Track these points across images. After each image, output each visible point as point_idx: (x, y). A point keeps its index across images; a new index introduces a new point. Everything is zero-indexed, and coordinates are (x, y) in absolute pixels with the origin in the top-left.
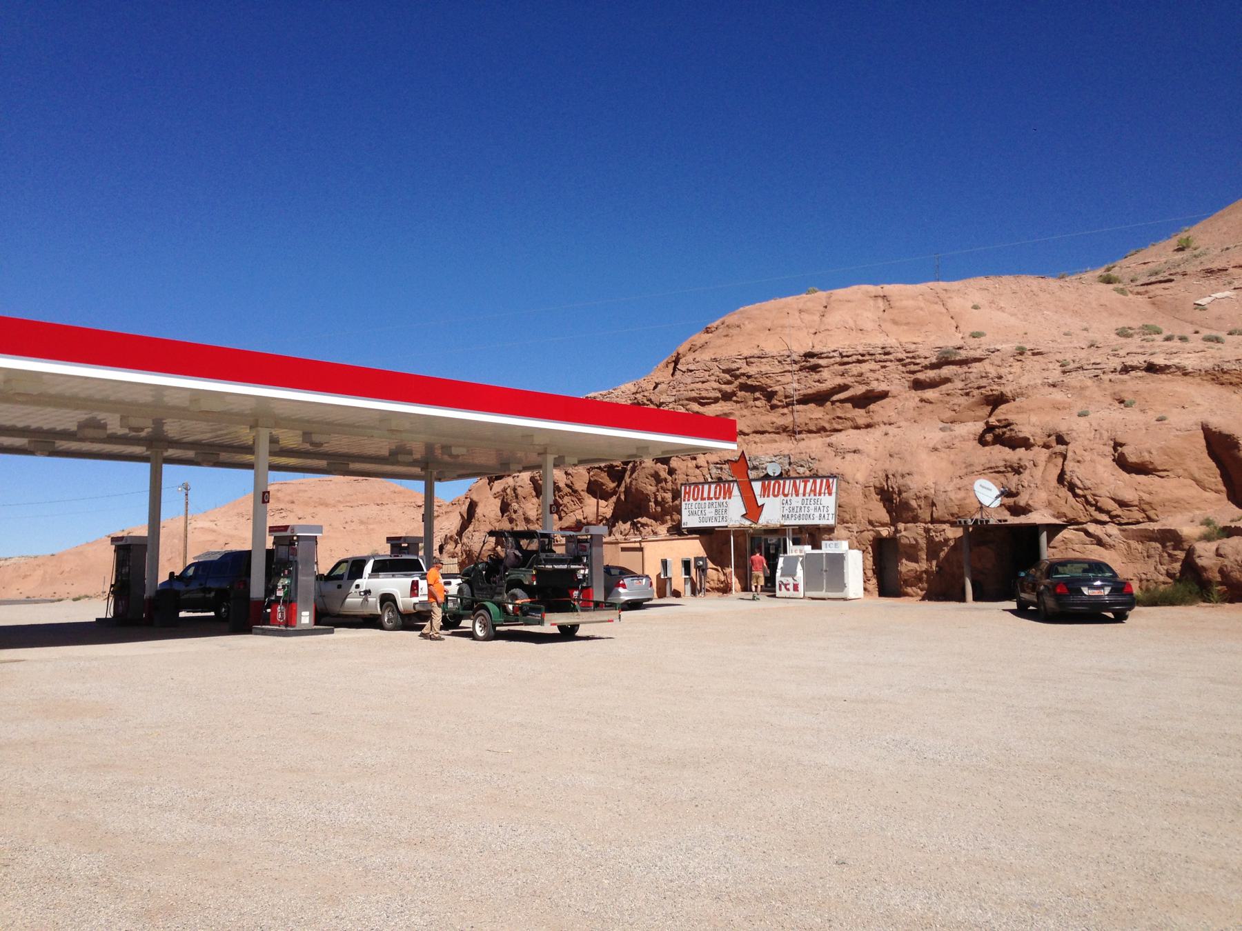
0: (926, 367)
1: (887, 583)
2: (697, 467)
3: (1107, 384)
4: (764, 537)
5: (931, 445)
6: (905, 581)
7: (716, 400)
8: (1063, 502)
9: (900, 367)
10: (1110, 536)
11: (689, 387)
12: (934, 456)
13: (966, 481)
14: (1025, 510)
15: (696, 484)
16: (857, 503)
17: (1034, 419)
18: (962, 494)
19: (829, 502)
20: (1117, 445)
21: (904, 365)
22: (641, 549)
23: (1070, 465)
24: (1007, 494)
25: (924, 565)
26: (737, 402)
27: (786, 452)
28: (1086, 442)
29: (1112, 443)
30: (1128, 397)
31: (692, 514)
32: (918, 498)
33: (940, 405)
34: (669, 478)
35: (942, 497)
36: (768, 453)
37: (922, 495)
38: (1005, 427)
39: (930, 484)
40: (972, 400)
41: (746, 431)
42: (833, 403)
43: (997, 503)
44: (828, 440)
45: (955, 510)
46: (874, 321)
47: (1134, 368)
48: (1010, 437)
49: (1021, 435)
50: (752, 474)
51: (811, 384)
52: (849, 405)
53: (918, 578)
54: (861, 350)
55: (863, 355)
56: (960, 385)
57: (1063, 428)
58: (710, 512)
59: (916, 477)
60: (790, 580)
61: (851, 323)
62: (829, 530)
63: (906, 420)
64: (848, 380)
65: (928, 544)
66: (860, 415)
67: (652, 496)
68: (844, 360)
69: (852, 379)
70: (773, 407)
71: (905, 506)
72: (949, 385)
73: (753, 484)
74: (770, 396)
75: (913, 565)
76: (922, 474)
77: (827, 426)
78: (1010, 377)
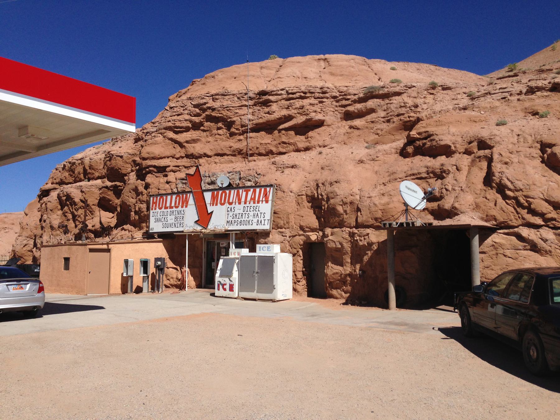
0: (355, 102)
1: (315, 284)
2: (168, 182)
3: (515, 103)
4: (217, 241)
5: (358, 158)
6: (330, 283)
7: (187, 129)
8: (492, 204)
9: (334, 103)
10: (545, 241)
11: (168, 119)
12: (360, 167)
13: (389, 187)
14: (452, 213)
15: (167, 194)
16: (290, 211)
17: (453, 130)
18: (385, 199)
19: (266, 208)
20: (544, 146)
21: (337, 101)
22: (108, 250)
23: (497, 167)
24: (430, 197)
25: (348, 269)
26: (204, 131)
27: (237, 170)
28: (510, 146)
29: (539, 146)
30: (542, 110)
31: (157, 220)
32: (345, 204)
33: (366, 130)
34: (145, 191)
35: (367, 202)
36: (221, 172)
37: (348, 200)
38: (425, 138)
39: (356, 190)
40: (392, 125)
41: (209, 153)
42: (280, 131)
43: (423, 205)
44: (273, 160)
45: (379, 215)
46: (316, 73)
47: (539, 89)
48: (431, 147)
49: (442, 143)
50: (204, 186)
51: (262, 115)
52: (292, 133)
53: (342, 282)
54: (303, 89)
55: (305, 93)
56: (383, 114)
57: (485, 134)
58: (171, 219)
59: (343, 185)
60: (227, 281)
61: (298, 74)
62: (265, 234)
63: (338, 143)
64: (292, 112)
65: (352, 248)
66: (301, 141)
67: (133, 207)
68: (290, 96)
69: (296, 111)
70: (232, 135)
71: (332, 211)
72: (373, 115)
73: (205, 194)
74: (229, 125)
75: (338, 269)
76: (348, 182)
77: (274, 150)
78: (425, 106)
